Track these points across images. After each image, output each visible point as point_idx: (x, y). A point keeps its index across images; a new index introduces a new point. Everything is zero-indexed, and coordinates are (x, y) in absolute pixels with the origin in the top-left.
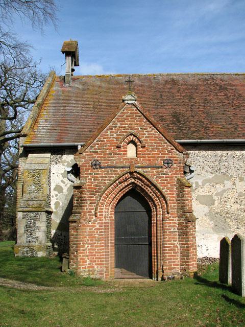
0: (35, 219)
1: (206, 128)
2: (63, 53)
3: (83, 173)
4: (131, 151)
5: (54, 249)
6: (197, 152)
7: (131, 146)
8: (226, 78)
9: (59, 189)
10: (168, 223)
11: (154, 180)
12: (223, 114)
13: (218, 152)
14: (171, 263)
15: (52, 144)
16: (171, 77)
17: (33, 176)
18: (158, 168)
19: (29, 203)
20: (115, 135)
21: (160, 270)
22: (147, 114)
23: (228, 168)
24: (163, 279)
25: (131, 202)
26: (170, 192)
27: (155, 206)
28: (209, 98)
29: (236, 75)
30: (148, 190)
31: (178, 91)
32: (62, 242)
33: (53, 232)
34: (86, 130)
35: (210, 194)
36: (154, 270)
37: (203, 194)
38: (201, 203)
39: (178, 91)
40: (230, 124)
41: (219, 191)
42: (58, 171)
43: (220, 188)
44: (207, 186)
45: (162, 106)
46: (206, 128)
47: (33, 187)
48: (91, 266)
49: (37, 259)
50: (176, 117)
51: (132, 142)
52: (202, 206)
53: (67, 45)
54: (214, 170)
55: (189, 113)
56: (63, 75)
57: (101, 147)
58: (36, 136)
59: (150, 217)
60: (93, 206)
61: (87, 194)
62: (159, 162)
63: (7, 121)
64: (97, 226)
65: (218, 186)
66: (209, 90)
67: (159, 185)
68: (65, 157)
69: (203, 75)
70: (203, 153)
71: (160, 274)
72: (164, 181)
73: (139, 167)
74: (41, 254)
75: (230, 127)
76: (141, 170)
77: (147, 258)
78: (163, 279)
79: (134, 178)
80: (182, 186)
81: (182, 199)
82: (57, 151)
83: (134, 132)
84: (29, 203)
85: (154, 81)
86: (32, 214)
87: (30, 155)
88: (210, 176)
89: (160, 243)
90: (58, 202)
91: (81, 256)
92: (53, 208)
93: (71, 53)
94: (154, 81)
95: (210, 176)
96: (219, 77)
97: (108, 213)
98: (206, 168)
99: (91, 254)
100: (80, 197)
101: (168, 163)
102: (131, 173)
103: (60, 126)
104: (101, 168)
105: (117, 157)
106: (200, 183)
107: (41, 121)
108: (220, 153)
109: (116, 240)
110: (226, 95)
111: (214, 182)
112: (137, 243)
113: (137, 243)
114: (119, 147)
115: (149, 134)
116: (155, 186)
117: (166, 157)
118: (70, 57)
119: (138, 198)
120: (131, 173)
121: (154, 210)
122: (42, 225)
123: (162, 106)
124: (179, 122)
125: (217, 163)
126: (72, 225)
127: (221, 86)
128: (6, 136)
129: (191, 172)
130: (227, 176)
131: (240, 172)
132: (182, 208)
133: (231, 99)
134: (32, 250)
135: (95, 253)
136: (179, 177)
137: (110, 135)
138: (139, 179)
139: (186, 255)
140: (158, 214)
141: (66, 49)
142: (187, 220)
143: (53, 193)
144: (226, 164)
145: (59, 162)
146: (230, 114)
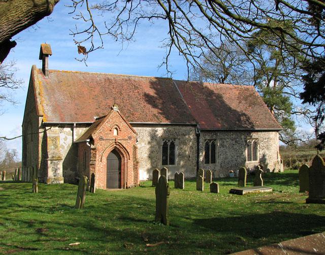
3: (95, 143)
11: (124, 145)
14: (130, 182)
17: (53, 140)
24: (127, 188)
25: (114, 157)
26: (130, 151)
27: (124, 157)
31: (113, 88)
34: (73, 113)
36: (122, 184)
39: (113, 88)
40: (143, 112)
51: (116, 128)
53: (48, 48)
62: (126, 138)
63: (223, 176)
64: (102, 166)
69: (124, 76)
71: (126, 186)
76: (119, 141)
82: (62, 126)
83: (117, 124)
85: (98, 79)
94: (98, 79)
101: (130, 138)
102: (116, 142)
115: (123, 125)
117: (129, 135)
121: (122, 160)
138: (118, 145)
139: (136, 177)
140: (125, 160)
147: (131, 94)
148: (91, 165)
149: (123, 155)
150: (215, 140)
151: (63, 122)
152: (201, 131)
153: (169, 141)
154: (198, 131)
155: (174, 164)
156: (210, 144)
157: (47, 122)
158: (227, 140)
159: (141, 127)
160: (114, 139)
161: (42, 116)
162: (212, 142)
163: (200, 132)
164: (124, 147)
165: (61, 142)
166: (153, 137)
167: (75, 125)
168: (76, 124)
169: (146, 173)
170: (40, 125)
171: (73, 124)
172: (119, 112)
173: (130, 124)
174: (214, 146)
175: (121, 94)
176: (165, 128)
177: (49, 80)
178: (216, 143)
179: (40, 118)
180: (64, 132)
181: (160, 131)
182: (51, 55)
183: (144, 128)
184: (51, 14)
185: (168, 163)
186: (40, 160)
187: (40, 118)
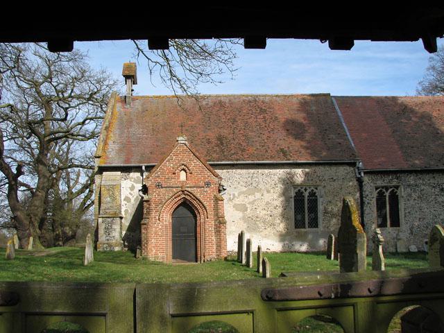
0: (112, 223)
1: (243, 150)
2: (124, 76)
3: (150, 191)
4: (183, 176)
5: (125, 246)
6: (234, 170)
7: (183, 172)
8: (267, 100)
9: (127, 199)
10: (207, 224)
11: (198, 196)
12: (259, 137)
13: (250, 170)
14: (209, 250)
15: (122, 165)
16: (219, 99)
18: (201, 187)
19: (107, 211)
20: (172, 165)
21: (202, 256)
22: (194, 150)
23: (258, 183)
24: (204, 261)
25: (184, 211)
26: (209, 204)
28: (249, 121)
29: (276, 96)
30: (194, 203)
32: (134, 239)
33: (124, 233)
34: (147, 151)
35: (244, 203)
36: (199, 256)
37: (239, 203)
38: (237, 210)
40: (263, 146)
41: (251, 200)
42: (128, 189)
43: (251, 198)
44: (242, 197)
45: (209, 129)
46: (243, 150)
47: (109, 199)
48: (156, 254)
49: (115, 252)
50: (220, 139)
51: (184, 170)
52: (238, 212)
54: (247, 185)
55: (231, 136)
56: (124, 95)
57: (162, 173)
58: (107, 157)
59: (196, 221)
60: (157, 214)
61: (153, 206)
62: (202, 184)
64: (160, 227)
65: (250, 197)
66: (251, 112)
67: (201, 199)
68: (132, 174)
69: (247, 96)
70: (239, 171)
72: (205, 196)
73: (188, 187)
74: (117, 249)
75: (262, 149)
76: (189, 189)
77: (237, 315)
78: (204, 261)
79: (185, 194)
80: (217, 200)
81: (217, 209)
82: (126, 170)
84: (107, 211)
86: (109, 220)
87: (104, 173)
88: (245, 189)
89: (203, 238)
90: (127, 210)
91: (149, 247)
92: (123, 214)
93: (130, 77)
95: (245, 189)
96: (261, 98)
97: (167, 218)
98: (241, 183)
99: (156, 246)
100: (148, 208)
101: (208, 184)
102: (182, 191)
103: (126, 147)
104: (162, 188)
105: (173, 180)
106: (236, 195)
107: (110, 142)
108: (252, 171)
109: (173, 236)
110: (264, 117)
111: (247, 194)
112: (187, 237)
113: (187, 237)
114: (174, 174)
115: (195, 164)
116: (199, 200)
118: (130, 80)
119: (187, 209)
120: (182, 191)
122: (117, 227)
123: (209, 129)
124: (222, 144)
125: (250, 179)
126: (143, 227)
127: (261, 109)
128: (57, 135)
129: (225, 190)
130: (257, 189)
131: (267, 186)
132: (217, 215)
133: (268, 122)
134: (110, 245)
135: (159, 243)
136: (215, 193)
137: (168, 165)
139: (220, 244)
140: (201, 218)
141: (127, 73)
142: (220, 223)
143: (123, 203)
144: (257, 179)
145: (128, 179)
146: (265, 137)
147: (249, 121)
150: (397, 187)
152: (365, 173)
153: (306, 190)
154: (360, 174)
155: (317, 227)
156: (387, 194)
157: (105, 165)
158: (423, 187)
159: (252, 168)
162: (390, 190)
163: (363, 175)
164: (197, 199)
165: (125, 192)
166: (288, 183)
167: (144, 168)
169: (277, 238)
171: (141, 167)
172: (188, 145)
173: (211, 165)
174: (394, 199)
175: (234, 121)
176: (307, 170)
177: (130, 110)
178: (398, 193)
180: (131, 179)
181: (299, 175)
183: (260, 171)
184: (348, 51)
185: (307, 226)
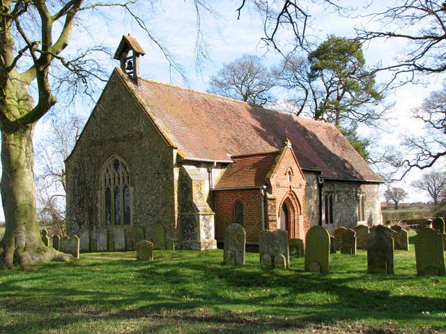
27: (294, 211)
121: (292, 215)
148: (272, 221)
149: (293, 208)
151: (225, 161)
160: (289, 186)
161: (176, 148)
168: (217, 163)
170: (174, 162)
179: (174, 151)
182: (143, 55)
186: (176, 215)
187: (174, 151)
